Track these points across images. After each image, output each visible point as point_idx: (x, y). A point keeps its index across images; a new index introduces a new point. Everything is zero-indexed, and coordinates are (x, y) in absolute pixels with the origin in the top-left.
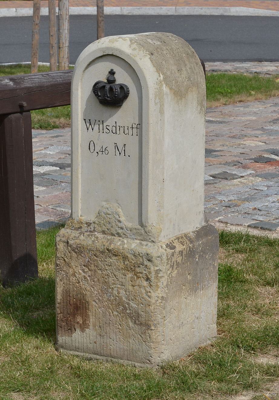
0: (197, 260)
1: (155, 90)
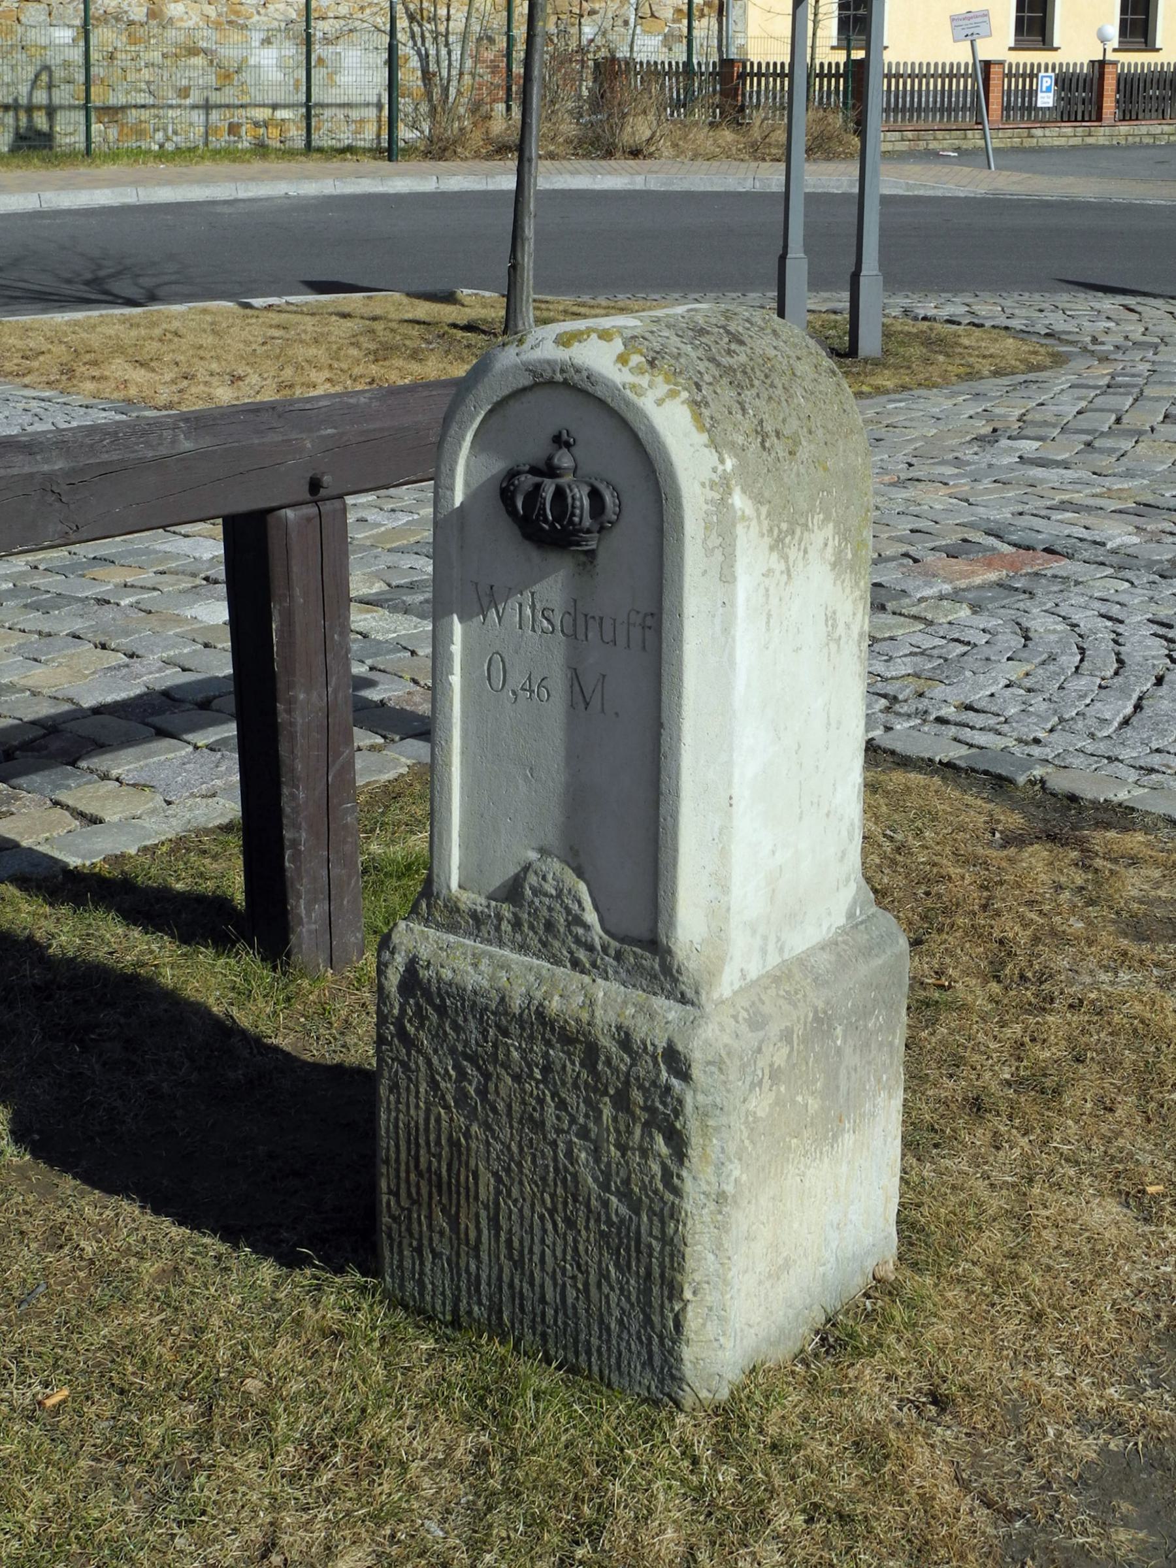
0: (839, 1043)
1: (705, 507)
